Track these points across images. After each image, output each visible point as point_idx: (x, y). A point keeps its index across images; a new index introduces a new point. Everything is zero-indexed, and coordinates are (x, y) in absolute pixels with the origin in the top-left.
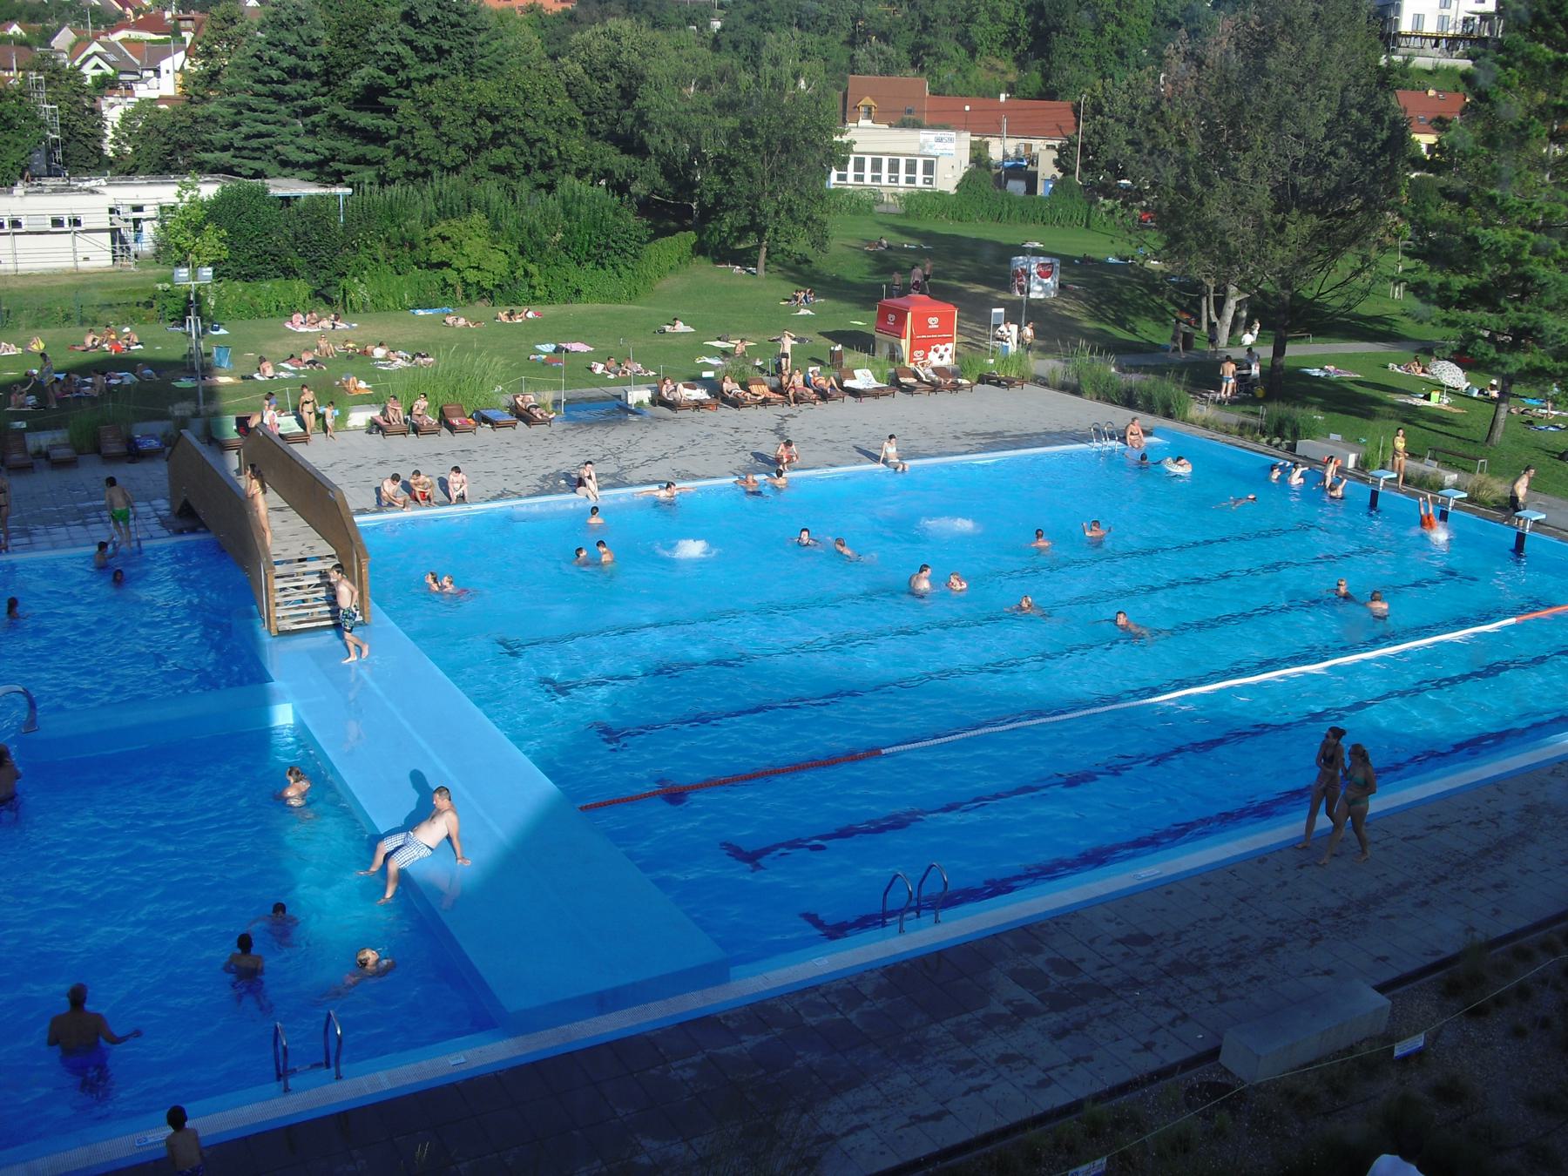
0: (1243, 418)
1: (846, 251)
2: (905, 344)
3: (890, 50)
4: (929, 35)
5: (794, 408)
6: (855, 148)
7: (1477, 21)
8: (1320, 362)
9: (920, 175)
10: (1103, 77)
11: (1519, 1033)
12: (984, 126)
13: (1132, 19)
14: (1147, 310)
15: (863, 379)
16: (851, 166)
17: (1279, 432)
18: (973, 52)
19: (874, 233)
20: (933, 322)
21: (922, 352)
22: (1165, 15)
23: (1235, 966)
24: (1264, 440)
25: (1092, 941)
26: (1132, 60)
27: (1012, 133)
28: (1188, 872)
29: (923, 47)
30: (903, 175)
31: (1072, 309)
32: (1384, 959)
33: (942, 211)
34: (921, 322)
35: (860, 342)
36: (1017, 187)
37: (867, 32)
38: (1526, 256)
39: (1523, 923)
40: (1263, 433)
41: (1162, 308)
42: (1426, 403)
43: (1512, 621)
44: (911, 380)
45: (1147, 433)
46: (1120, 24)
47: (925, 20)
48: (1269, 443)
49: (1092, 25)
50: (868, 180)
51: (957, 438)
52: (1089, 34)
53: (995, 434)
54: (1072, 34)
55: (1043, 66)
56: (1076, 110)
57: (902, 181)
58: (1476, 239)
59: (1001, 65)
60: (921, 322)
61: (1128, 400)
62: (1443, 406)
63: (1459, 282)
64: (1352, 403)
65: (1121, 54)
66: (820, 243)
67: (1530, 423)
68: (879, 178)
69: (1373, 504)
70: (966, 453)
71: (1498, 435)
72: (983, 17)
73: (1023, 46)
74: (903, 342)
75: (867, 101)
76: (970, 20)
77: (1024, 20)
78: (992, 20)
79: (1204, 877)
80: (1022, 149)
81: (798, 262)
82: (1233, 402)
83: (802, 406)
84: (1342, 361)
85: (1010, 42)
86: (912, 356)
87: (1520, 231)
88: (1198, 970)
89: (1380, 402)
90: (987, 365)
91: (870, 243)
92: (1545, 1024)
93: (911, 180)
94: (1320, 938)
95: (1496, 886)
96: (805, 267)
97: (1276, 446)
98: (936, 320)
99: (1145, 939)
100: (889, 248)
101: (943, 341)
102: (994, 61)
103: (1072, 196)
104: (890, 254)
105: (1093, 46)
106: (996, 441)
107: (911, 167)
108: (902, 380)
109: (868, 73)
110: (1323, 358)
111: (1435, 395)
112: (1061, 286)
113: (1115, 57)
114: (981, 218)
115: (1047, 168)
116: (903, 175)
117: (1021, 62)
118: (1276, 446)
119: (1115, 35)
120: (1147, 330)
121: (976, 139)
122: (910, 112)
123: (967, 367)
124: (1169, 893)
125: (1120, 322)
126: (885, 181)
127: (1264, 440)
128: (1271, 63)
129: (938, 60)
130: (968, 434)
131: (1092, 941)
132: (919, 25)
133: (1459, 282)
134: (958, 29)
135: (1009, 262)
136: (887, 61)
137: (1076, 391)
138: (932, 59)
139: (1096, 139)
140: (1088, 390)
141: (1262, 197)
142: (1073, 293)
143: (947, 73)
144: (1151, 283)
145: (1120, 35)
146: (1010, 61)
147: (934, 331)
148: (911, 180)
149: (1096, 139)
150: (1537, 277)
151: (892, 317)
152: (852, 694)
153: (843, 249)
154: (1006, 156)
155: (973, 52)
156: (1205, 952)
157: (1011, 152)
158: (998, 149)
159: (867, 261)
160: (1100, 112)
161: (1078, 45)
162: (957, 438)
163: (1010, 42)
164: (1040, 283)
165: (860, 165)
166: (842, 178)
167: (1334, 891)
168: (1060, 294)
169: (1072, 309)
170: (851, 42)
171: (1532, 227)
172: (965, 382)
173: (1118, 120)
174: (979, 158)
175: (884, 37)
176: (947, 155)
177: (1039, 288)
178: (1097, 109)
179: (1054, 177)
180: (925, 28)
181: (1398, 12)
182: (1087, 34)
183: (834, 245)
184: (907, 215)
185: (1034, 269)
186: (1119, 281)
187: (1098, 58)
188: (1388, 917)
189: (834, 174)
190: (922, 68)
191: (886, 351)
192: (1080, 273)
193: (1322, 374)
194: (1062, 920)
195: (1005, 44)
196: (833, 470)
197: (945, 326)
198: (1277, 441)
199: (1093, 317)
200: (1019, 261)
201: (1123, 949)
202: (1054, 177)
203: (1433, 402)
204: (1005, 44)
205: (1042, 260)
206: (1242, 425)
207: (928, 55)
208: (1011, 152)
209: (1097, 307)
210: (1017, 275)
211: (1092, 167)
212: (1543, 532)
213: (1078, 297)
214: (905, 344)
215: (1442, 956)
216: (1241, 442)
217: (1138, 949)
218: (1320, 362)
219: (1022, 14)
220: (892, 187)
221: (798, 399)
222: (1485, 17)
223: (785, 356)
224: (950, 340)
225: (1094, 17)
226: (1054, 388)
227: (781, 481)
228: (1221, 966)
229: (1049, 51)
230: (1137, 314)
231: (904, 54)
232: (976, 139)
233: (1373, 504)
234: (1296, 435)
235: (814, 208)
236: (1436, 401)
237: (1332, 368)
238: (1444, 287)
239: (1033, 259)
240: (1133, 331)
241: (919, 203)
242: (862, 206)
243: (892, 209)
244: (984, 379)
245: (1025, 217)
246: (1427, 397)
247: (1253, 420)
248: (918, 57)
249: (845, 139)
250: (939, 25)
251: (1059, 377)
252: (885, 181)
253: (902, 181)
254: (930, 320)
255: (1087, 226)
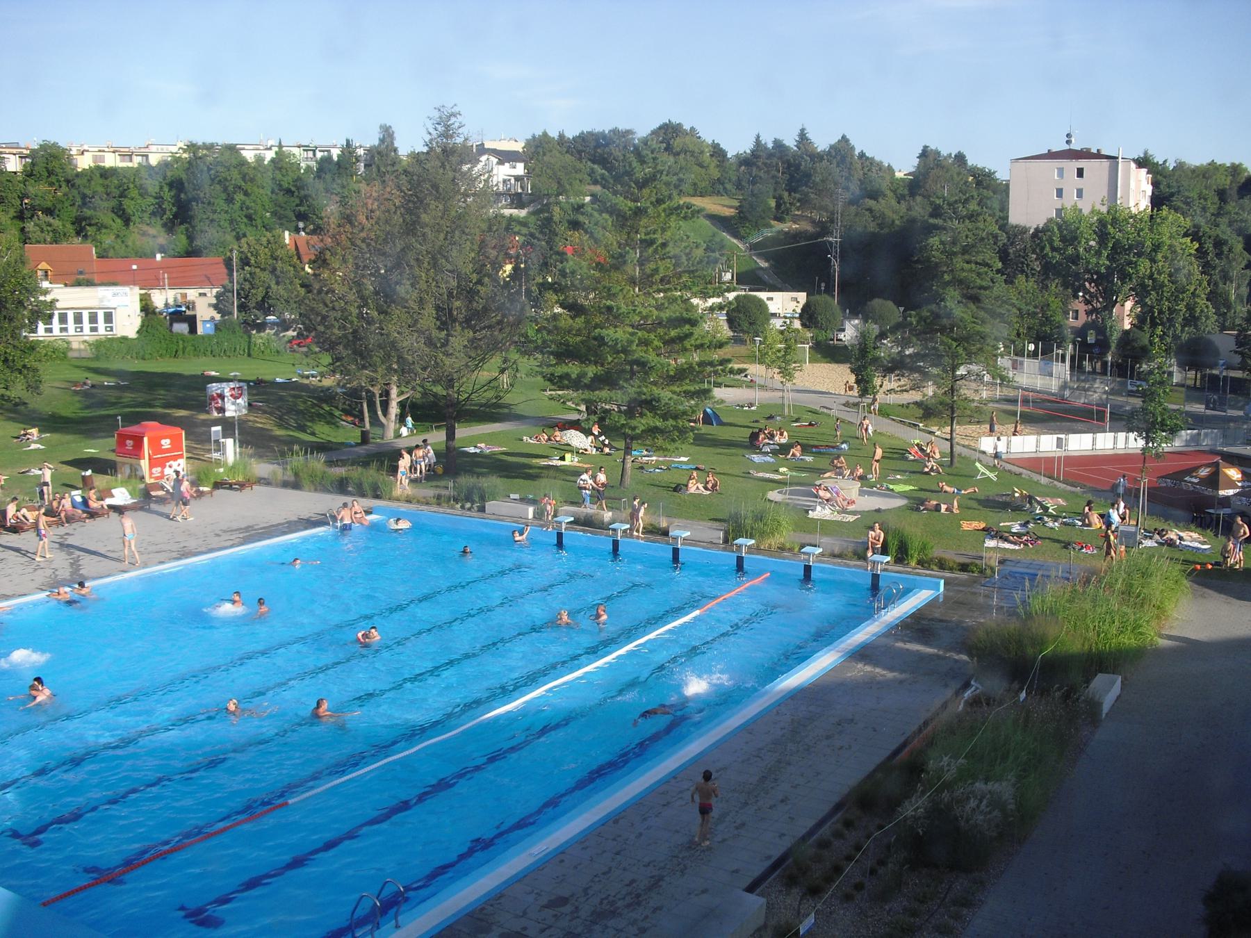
0: (438, 492)
1: (56, 392)
2: (144, 464)
3: (56, 223)
4: (89, 208)
5: (67, 528)
6: (58, 305)
7: (513, 181)
8: (473, 441)
9: (101, 325)
10: (238, 238)
11: (848, 898)
12: (149, 281)
13: (255, 188)
14: (320, 416)
15: (121, 496)
16: (56, 319)
17: (468, 498)
18: (127, 221)
19: (79, 375)
20: (166, 443)
21: (159, 469)
22: (280, 185)
23: (639, 904)
24: (458, 506)
25: (525, 913)
26: (259, 221)
27: (173, 285)
28: (567, 842)
29: (85, 219)
30: (86, 325)
31: (262, 422)
32: (736, 871)
33: (128, 353)
34: (155, 445)
35: (103, 467)
36: (181, 328)
37: (33, 209)
38: (634, 347)
39: (810, 823)
40: (456, 500)
41: (332, 415)
42: (561, 463)
43: (697, 613)
44: (161, 493)
45: (368, 512)
46: (246, 194)
47: (84, 197)
48: (463, 507)
49: (224, 196)
50: (56, 331)
51: (218, 535)
52: (222, 202)
53: (247, 529)
54: (209, 203)
55: (187, 230)
56: (228, 263)
57: (87, 330)
58: (603, 338)
59: (152, 231)
60: (155, 445)
61: (341, 487)
62: (575, 464)
63: (591, 371)
64: (515, 469)
65: (250, 217)
66: (34, 387)
67: (642, 468)
68: (65, 330)
69: (560, 544)
70: (232, 546)
71: (628, 480)
72: (134, 193)
73: (169, 215)
74: (142, 462)
75: (44, 265)
76: (122, 195)
77: (168, 195)
78: (141, 195)
79: (583, 841)
80: (179, 297)
81: (16, 405)
82: (428, 478)
83: (74, 525)
84: (488, 439)
85: (158, 211)
86: (151, 473)
87: (631, 330)
88: (614, 913)
89: (530, 467)
90: (219, 473)
91: (75, 384)
92: (859, 887)
93: (94, 329)
94: (686, 868)
95: (782, 801)
96: (22, 408)
97: (469, 509)
98: (168, 441)
99: (563, 901)
100: (93, 386)
101: (175, 458)
102: (145, 228)
103: (234, 332)
104: (94, 391)
105: (226, 212)
106: (251, 534)
107: (93, 319)
108: (153, 493)
109: (39, 242)
110: (476, 438)
111: (568, 456)
112: (250, 405)
113: (245, 220)
114: (161, 356)
115: (205, 313)
116: (86, 325)
117: (170, 227)
118: (469, 509)
119: (243, 203)
120: (323, 432)
121: (143, 292)
122: (81, 273)
123: (202, 476)
124: (562, 861)
125: (302, 428)
126: (71, 331)
127: (458, 506)
128: (425, 218)
129: (99, 230)
130: (225, 531)
131: (525, 913)
132: (79, 202)
133: (591, 371)
134: (113, 203)
135: (205, 389)
136: (54, 231)
137: (296, 485)
138: (94, 228)
139: (247, 286)
140: (306, 483)
141: (428, 319)
142: (259, 408)
143: (108, 239)
144: (325, 396)
145: (248, 203)
146: (159, 227)
147: (168, 451)
148: (94, 329)
149: (247, 286)
150: (648, 362)
151: (130, 443)
152: (213, 764)
153: (53, 391)
154: (167, 305)
155: (127, 221)
156: (611, 898)
157: (171, 301)
158: (161, 298)
159: (77, 398)
160: (248, 264)
161: (214, 212)
162: (218, 535)
163: (158, 211)
164: (233, 404)
165: (63, 319)
166: (49, 330)
167: (677, 832)
168: (249, 410)
169: (262, 422)
170: (20, 217)
171: (638, 327)
172: (206, 489)
173: (263, 270)
174: (147, 309)
175: (49, 212)
176: (121, 309)
177: (233, 408)
178: (245, 262)
179: (213, 318)
180: (84, 204)
181: (427, 182)
182: (221, 203)
183: (46, 388)
184: (97, 358)
185: (227, 393)
186: (295, 396)
187: (231, 221)
188: (724, 840)
189: (41, 327)
190: (86, 237)
191: (128, 471)
192: (258, 389)
193: (478, 451)
194: (497, 898)
195: (153, 214)
196: (126, 575)
197: (176, 446)
198: (468, 505)
199: (280, 426)
200: (214, 388)
201: (551, 912)
202: (213, 318)
203: (567, 462)
204: (153, 214)
205: (232, 385)
206: (439, 497)
207: (90, 225)
208: (171, 301)
209: (281, 418)
210: (213, 398)
211: (248, 308)
212: (690, 545)
213: (265, 412)
214: (144, 464)
215: (773, 860)
216: (441, 510)
217: (562, 909)
218: (473, 441)
219: (166, 189)
220: (79, 338)
221: (70, 519)
222: (518, 178)
223: (46, 484)
224: (181, 456)
225: (225, 190)
226: (277, 486)
227: (84, 591)
228: (628, 906)
229: (192, 217)
230: (312, 421)
231: (69, 226)
232: (143, 292)
233: (560, 544)
234: (483, 499)
235: (22, 360)
236: (570, 460)
237: (483, 445)
238: (582, 375)
239: (224, 385)
240: (313, 434)
241: (105, 347)
242: (59, 353)
243: (83, 355)
244: (218, 485)
245: (197, 352)
246: (563, 459)
247: (444, 492)
248: (81, 227)
249: (48, 298)
250: (97, 201)
251: (280, 476)
252: (71, 331)
253: (87, 330)
254: (163, 442)
255: (249, 355)
